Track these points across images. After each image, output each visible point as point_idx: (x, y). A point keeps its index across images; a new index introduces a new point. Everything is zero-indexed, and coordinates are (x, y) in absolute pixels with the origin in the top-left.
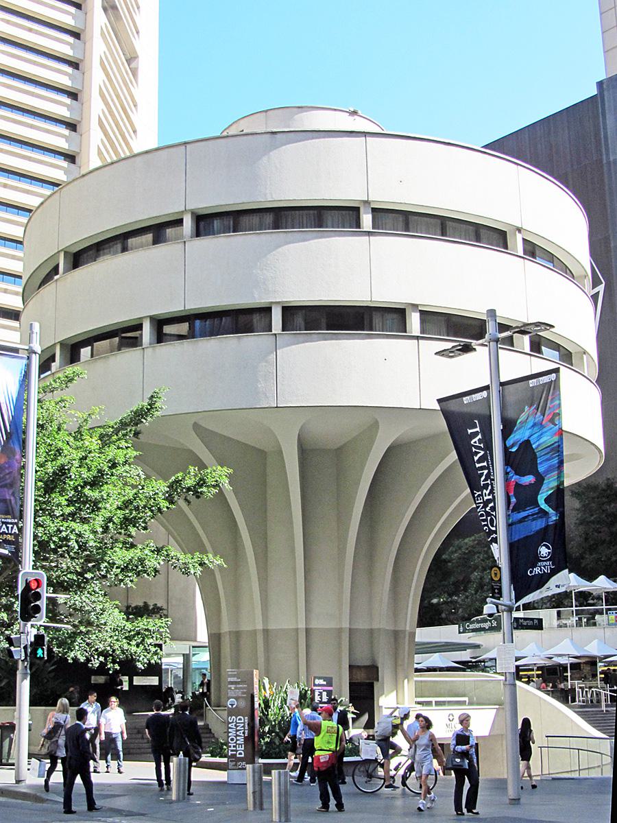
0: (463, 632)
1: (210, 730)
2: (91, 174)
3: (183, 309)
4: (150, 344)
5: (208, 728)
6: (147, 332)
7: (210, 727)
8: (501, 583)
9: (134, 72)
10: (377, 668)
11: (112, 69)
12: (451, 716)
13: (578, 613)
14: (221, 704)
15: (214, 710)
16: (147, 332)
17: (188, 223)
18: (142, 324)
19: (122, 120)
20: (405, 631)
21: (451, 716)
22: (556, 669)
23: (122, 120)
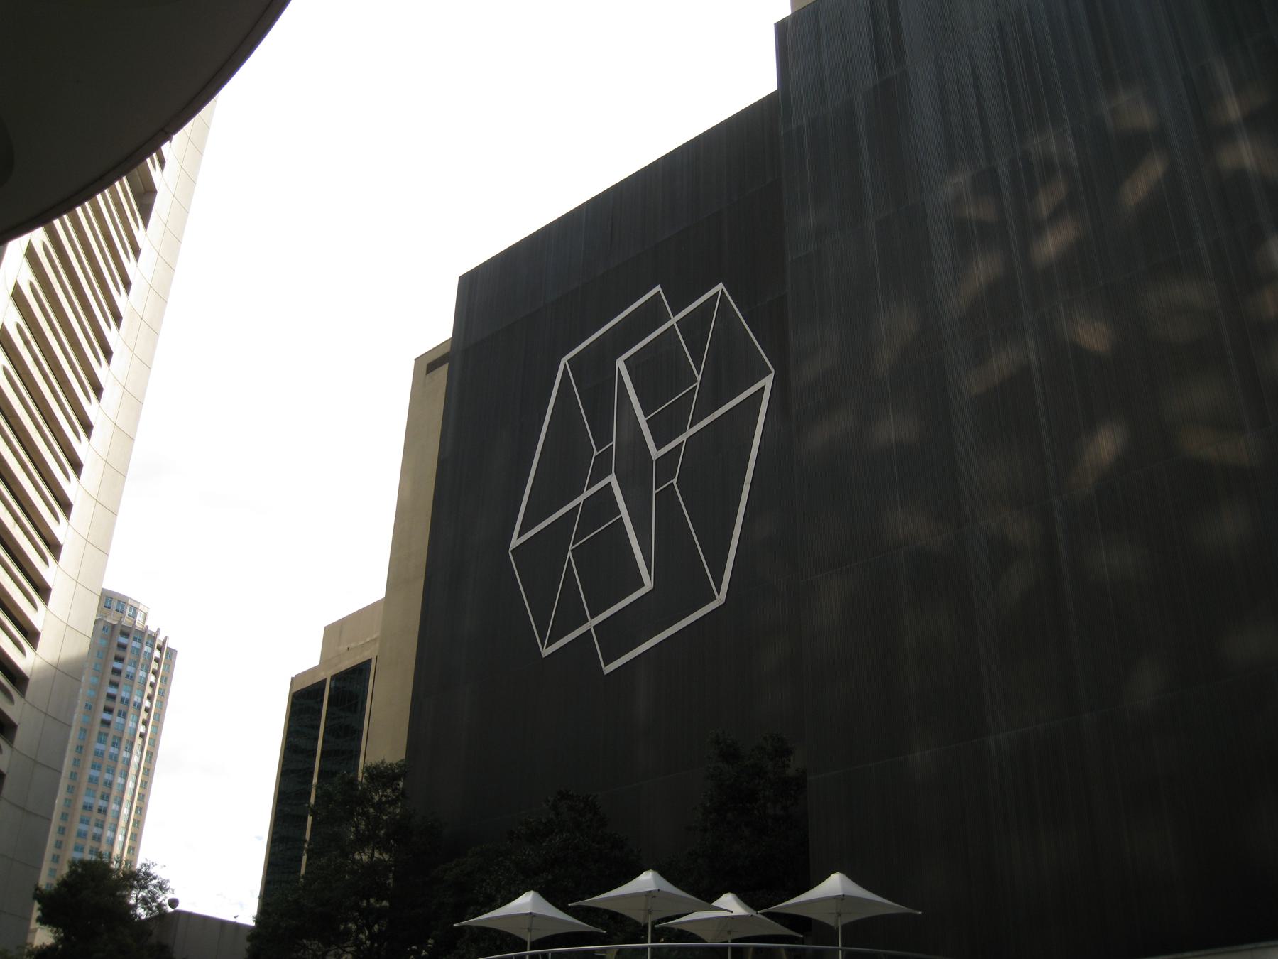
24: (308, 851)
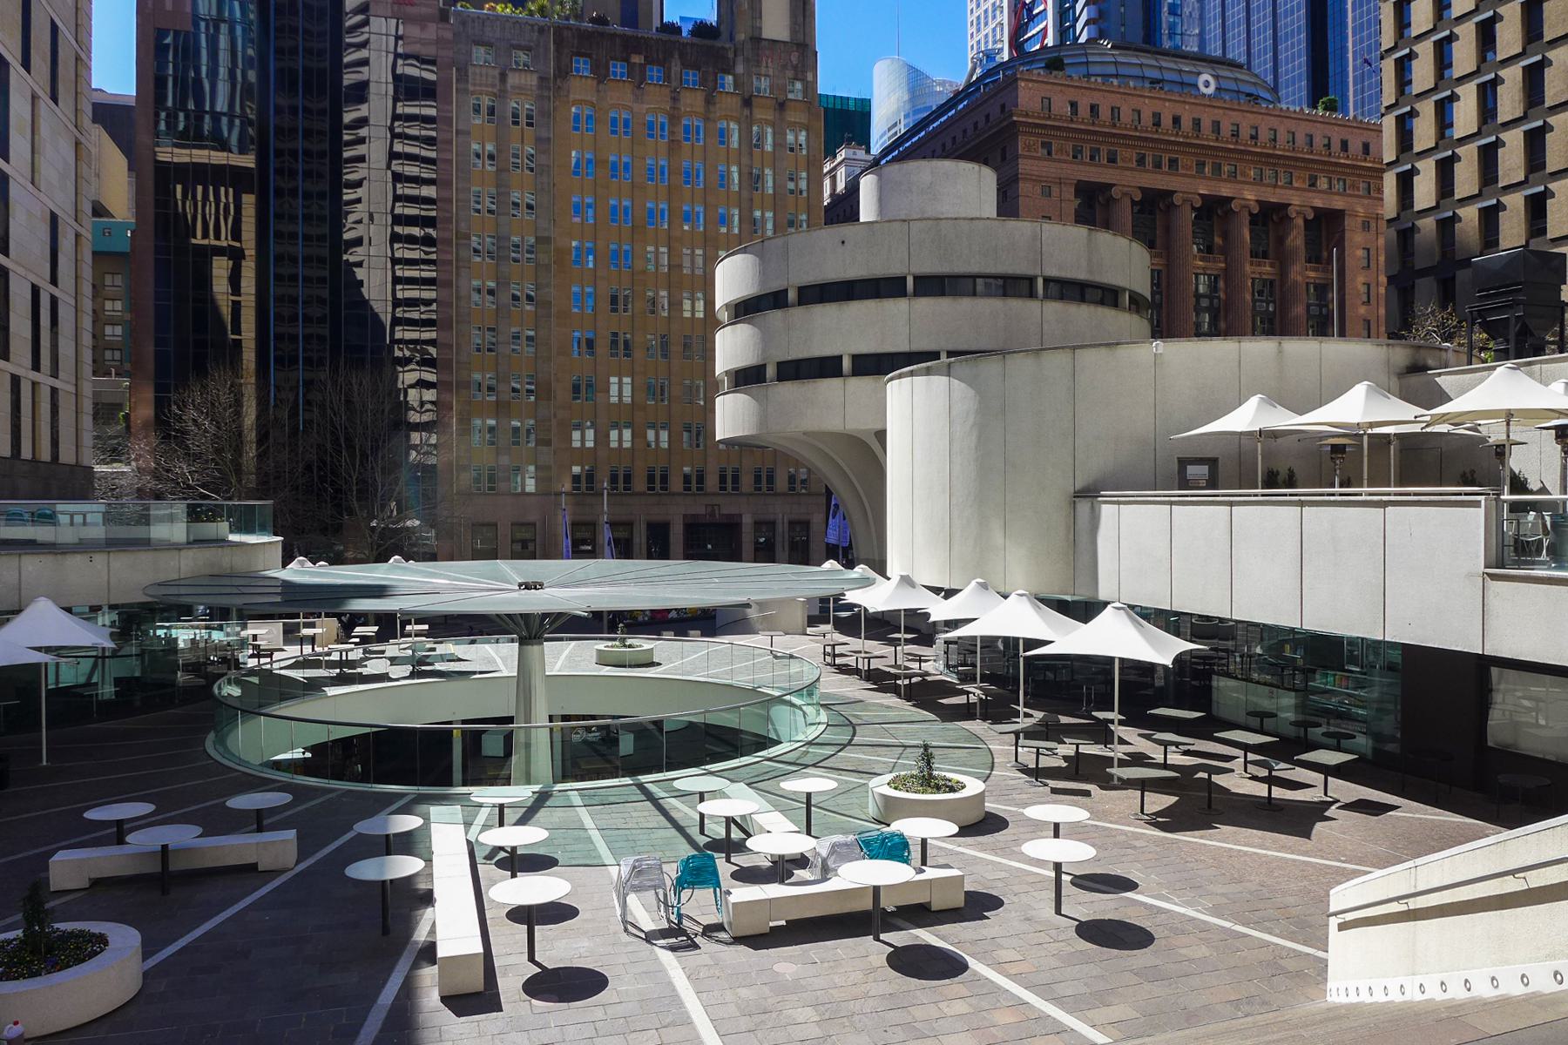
22: (450, 732)
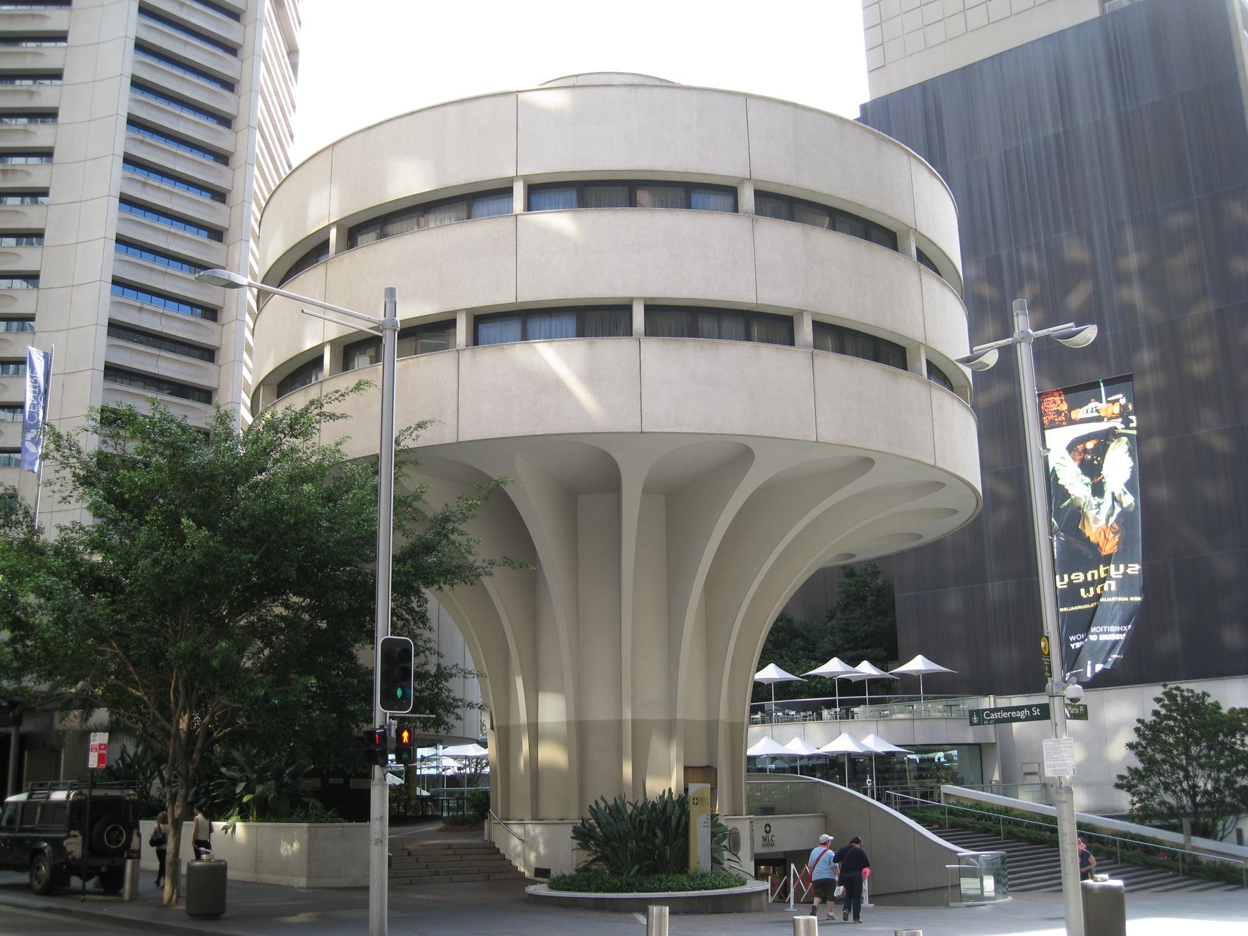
0: (979, 723)
1: (498, 849)
2: (413, 116)
3: (514, 301)
4: (466, 346)
5: (494, 847)
6: (462, 332)
7: (497, 846)
8: (1049, 658)
9: (294, 66)
10: (716, 770)
11: (272, 61)
12: (768, 827)
13: (842, 703)
14: (511, 817)
15: (505, 824)
16: (462, 332)
17: (519, 191)
18: (456, 319)
19: (280, 122)
20: (620, 723)
21: (768, 827)
23: (280, 122)
24: (854, 662)
